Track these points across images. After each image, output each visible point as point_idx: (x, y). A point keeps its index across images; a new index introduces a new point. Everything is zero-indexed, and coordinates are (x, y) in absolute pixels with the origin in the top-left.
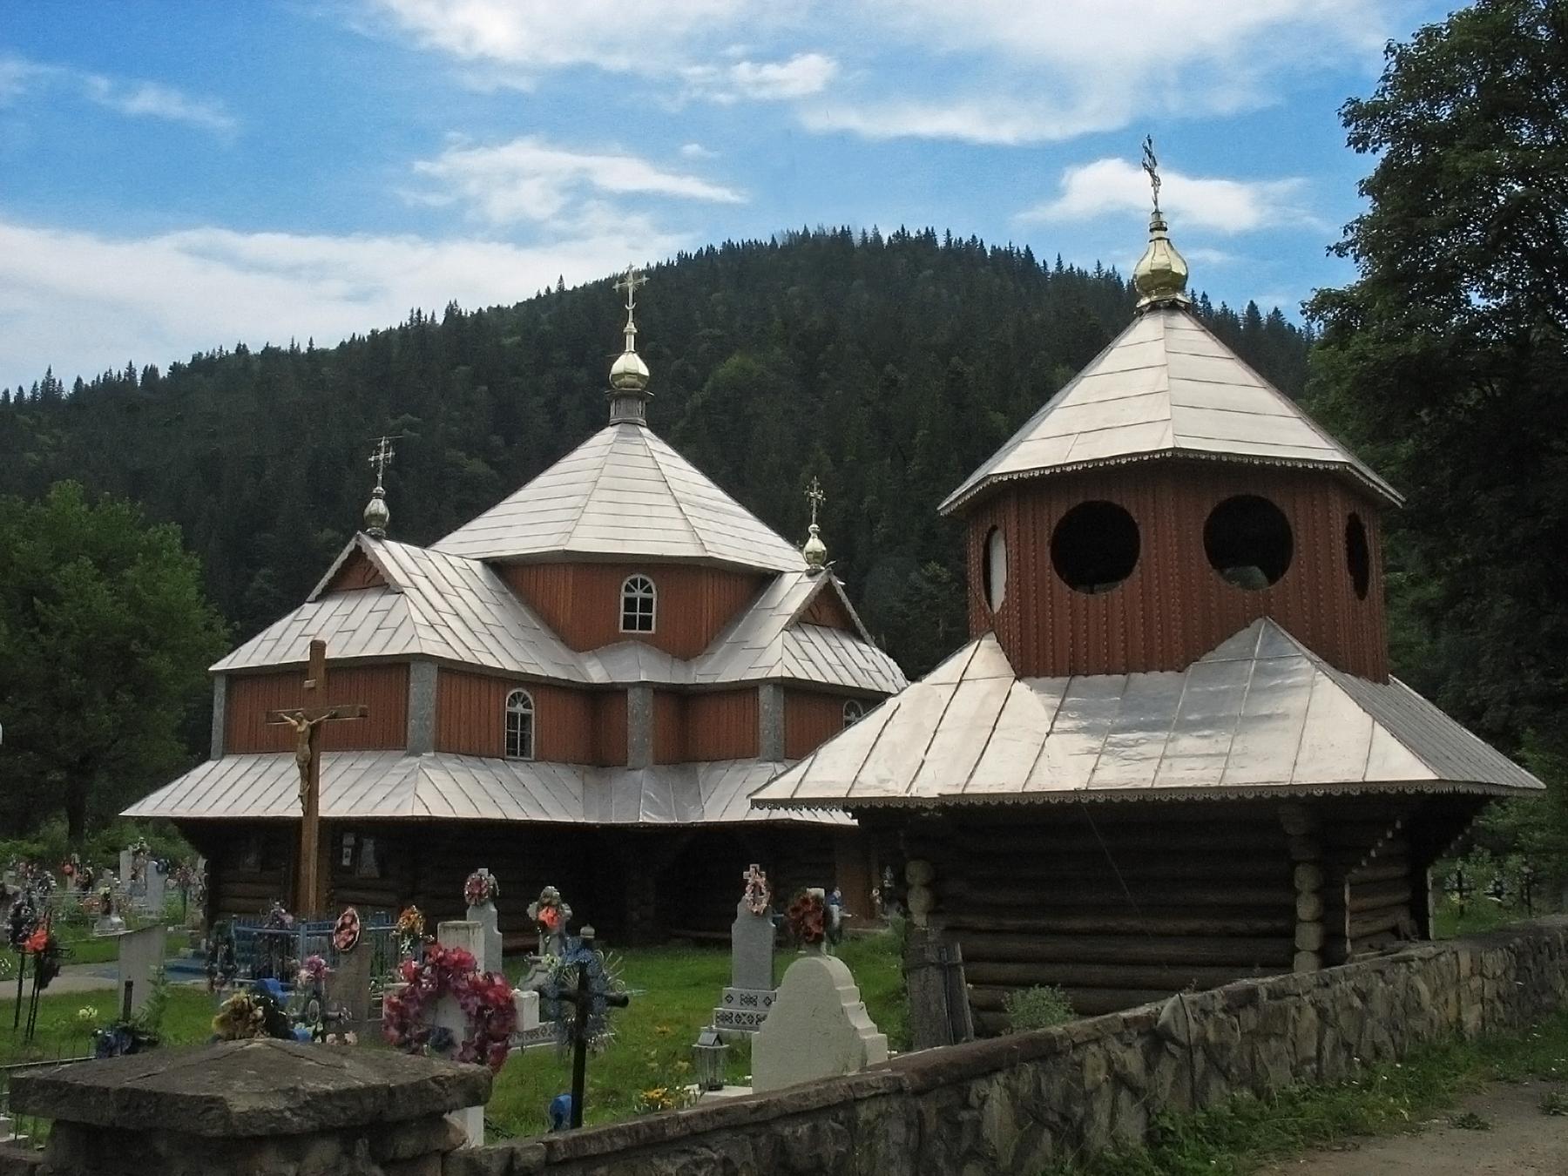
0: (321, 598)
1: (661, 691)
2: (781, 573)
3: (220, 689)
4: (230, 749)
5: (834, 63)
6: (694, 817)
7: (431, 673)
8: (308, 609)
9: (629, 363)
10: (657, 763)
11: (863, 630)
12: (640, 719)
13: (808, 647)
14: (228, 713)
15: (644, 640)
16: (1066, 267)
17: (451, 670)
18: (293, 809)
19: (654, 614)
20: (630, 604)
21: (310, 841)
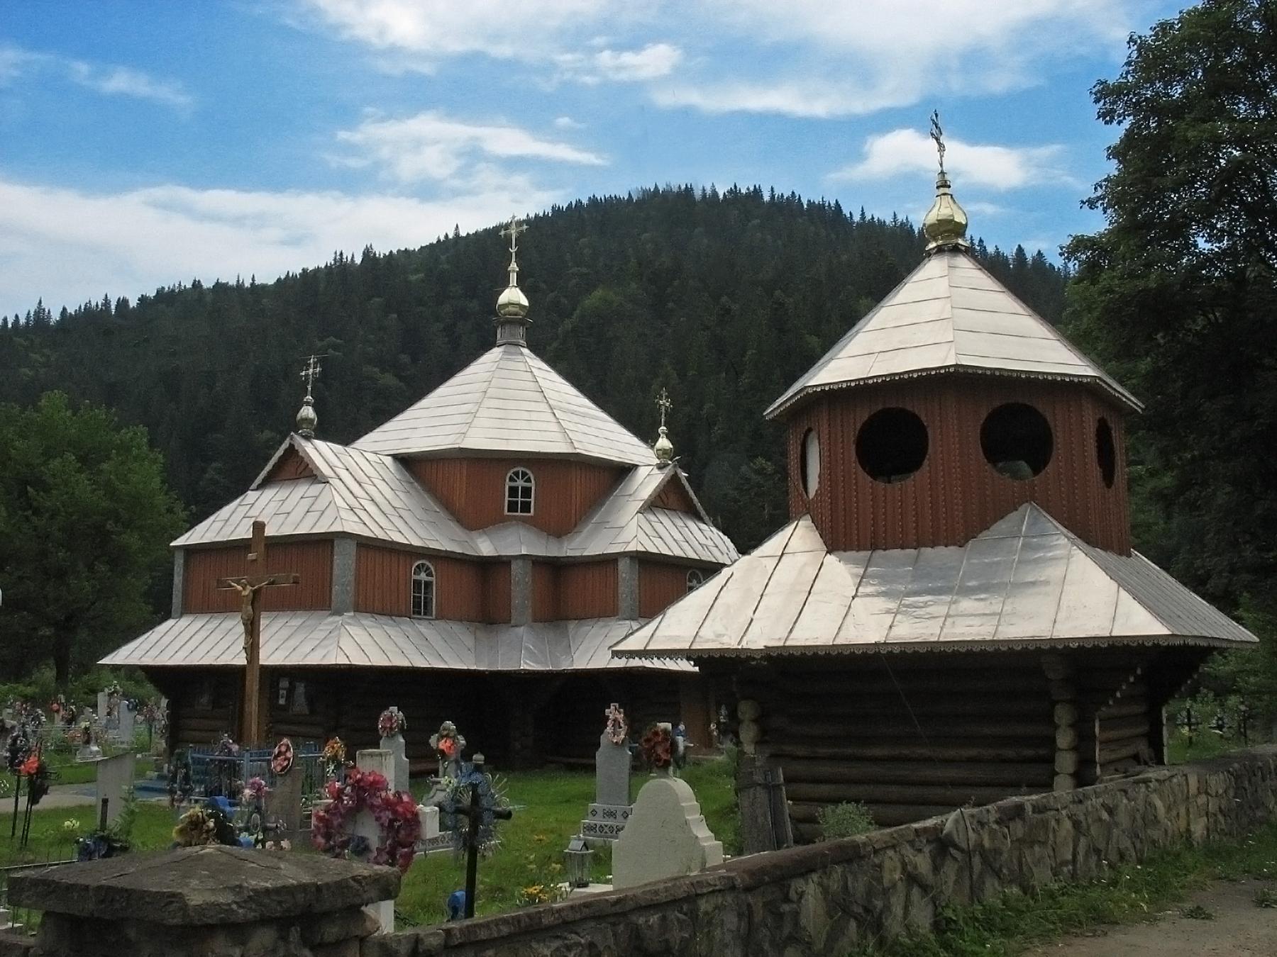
0: (261, 486)
1: (538, 563)
2: (636, 466)
3: (179, 561)
4: (187, 610)
5: (679, 52)
6: (565, 665)
7: (351, 548)
8: (251, 496)
9: (513, 295)
10: (535, 621)
11: (703, 513)
12: (521, 585)
13: (658, 526)
14: (186, 580)
15: (525, 521)
16: (868, 217)
17: (367, 546)
18: (238, 658)
19: (532, 500)
20: (513, 491)
21: (253, 685)
